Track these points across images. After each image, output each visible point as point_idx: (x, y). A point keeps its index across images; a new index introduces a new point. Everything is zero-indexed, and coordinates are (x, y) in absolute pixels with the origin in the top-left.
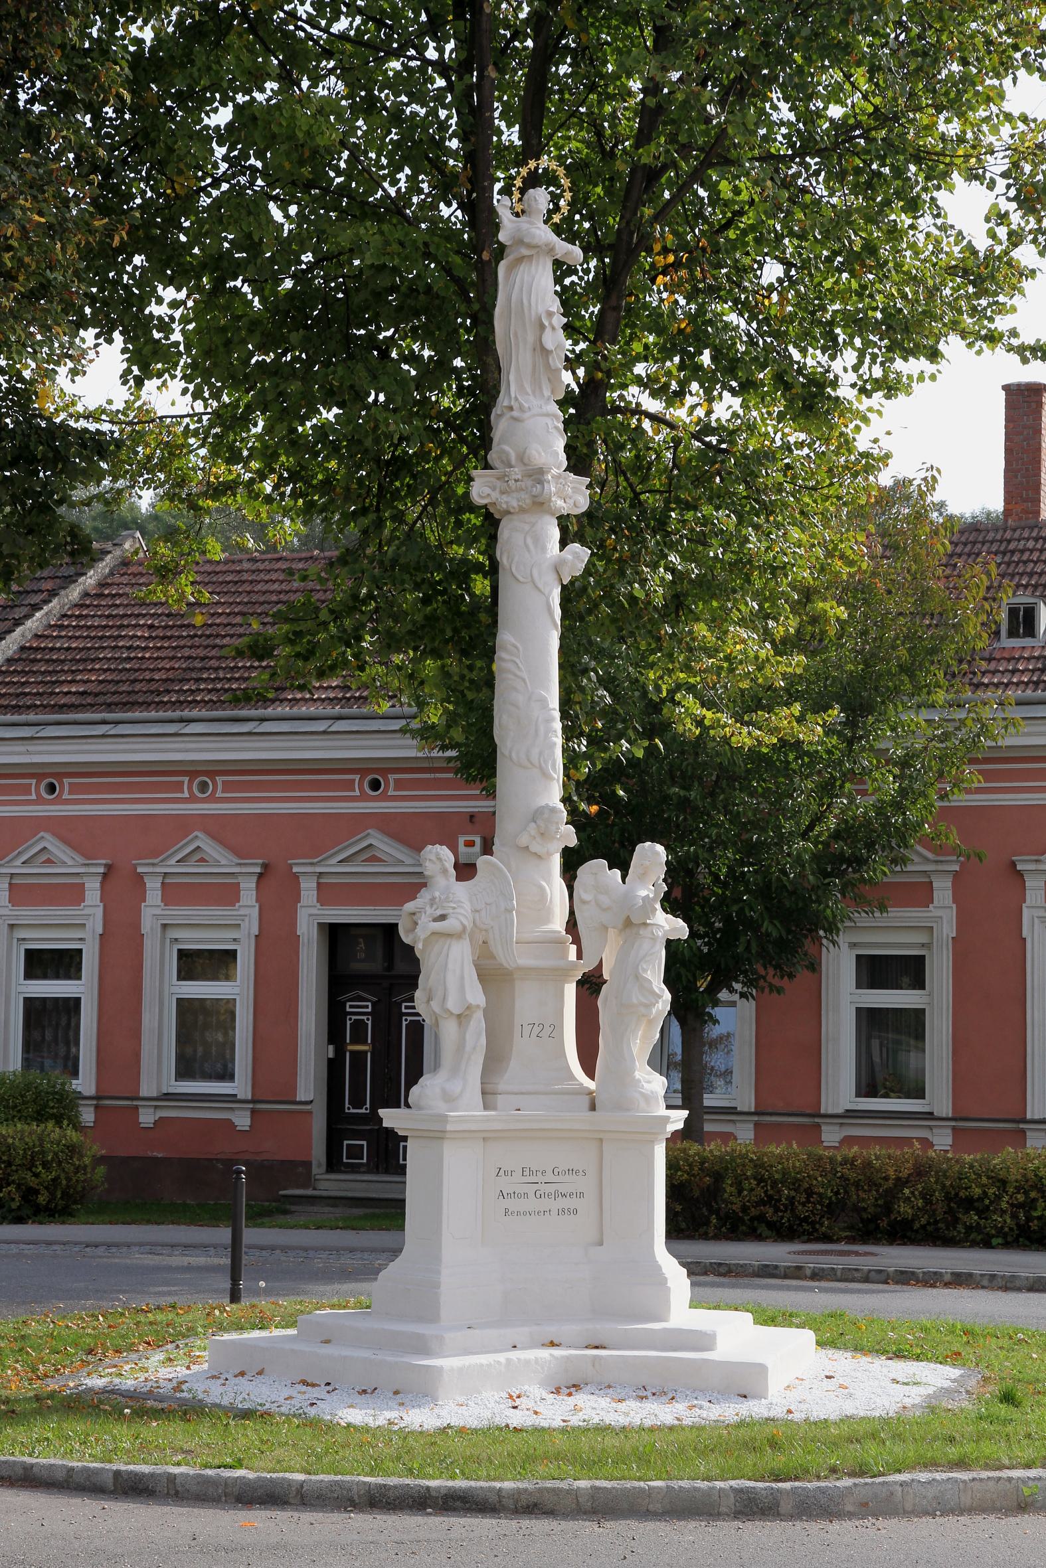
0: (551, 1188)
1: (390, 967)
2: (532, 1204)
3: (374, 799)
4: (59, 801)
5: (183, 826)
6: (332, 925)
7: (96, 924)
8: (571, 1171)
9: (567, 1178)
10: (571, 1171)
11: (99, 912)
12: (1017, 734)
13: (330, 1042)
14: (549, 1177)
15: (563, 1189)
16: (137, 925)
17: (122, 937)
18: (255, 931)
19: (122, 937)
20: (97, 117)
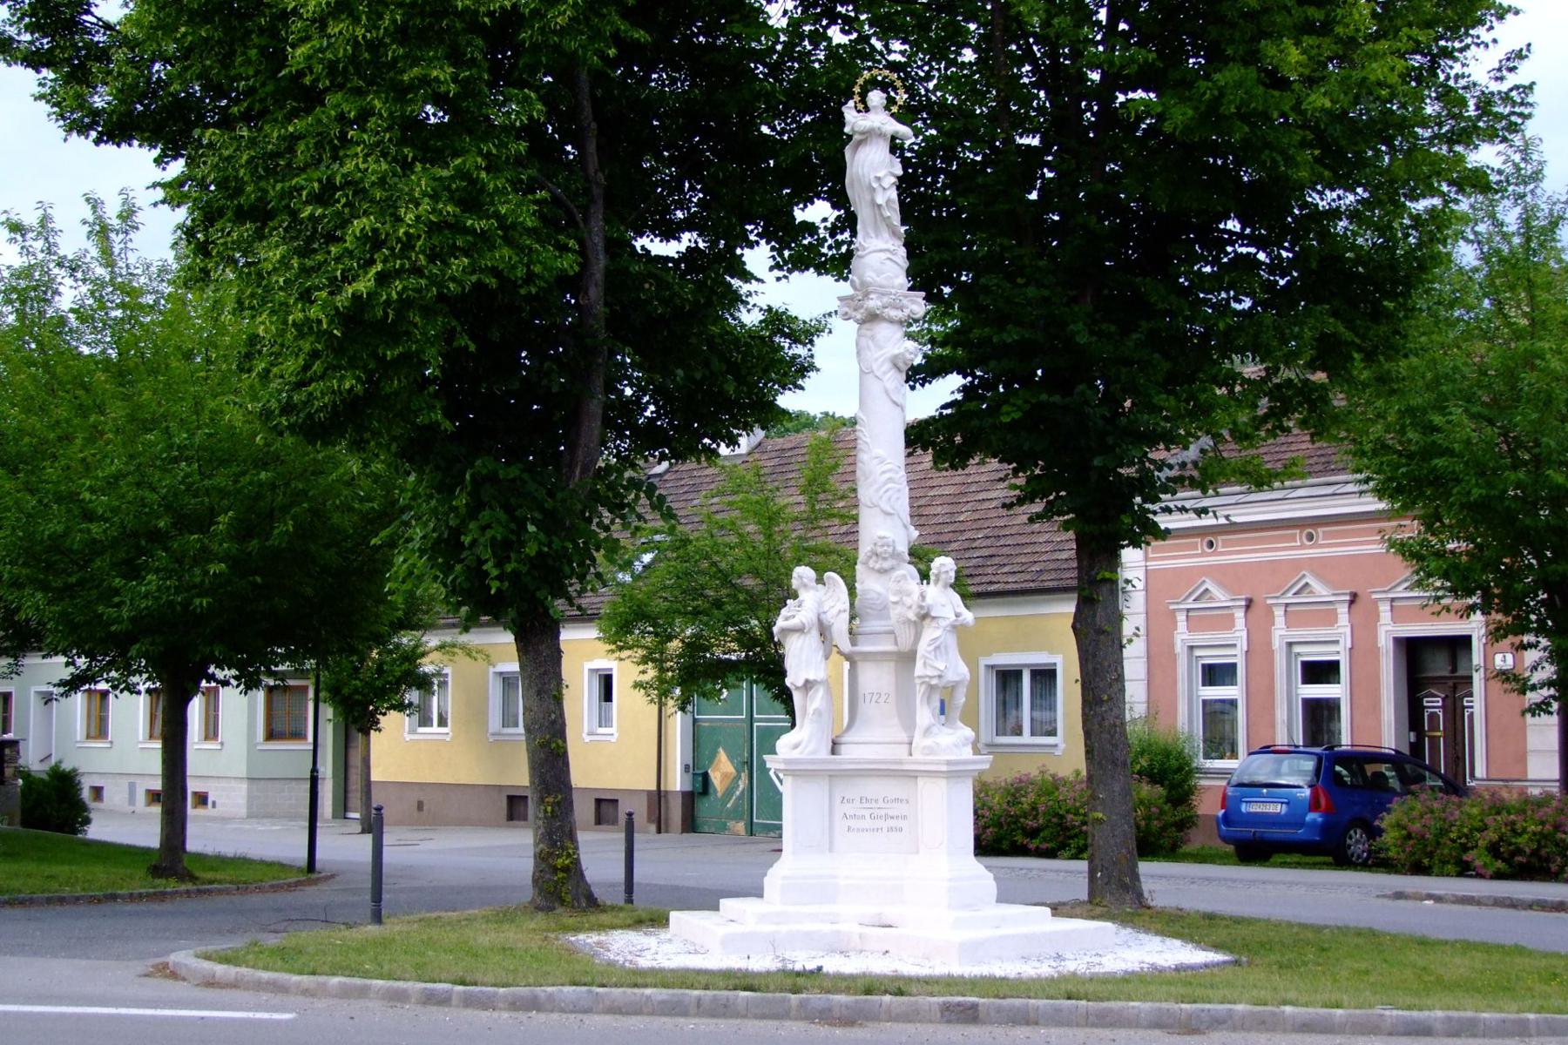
0: (883, 812)
1: (1454, 670)
2: (868, 823)
3: (1310, 547)
4: (1216, 553)
5: (1297, 565)
6: (1409, 639)
7: (1243, 645)
8: (897, 800)
9: (895, 805)
10: (897, 800)
11: (1244, 634)
12: (1217, 494)
13: (1411, 729)
14: (881, 804)
15: (891, 813)
16: (1269, 643)
17: (1259, 649)
18: (1349, 645)
19: (1259, 649)
20: (1099, 43)
